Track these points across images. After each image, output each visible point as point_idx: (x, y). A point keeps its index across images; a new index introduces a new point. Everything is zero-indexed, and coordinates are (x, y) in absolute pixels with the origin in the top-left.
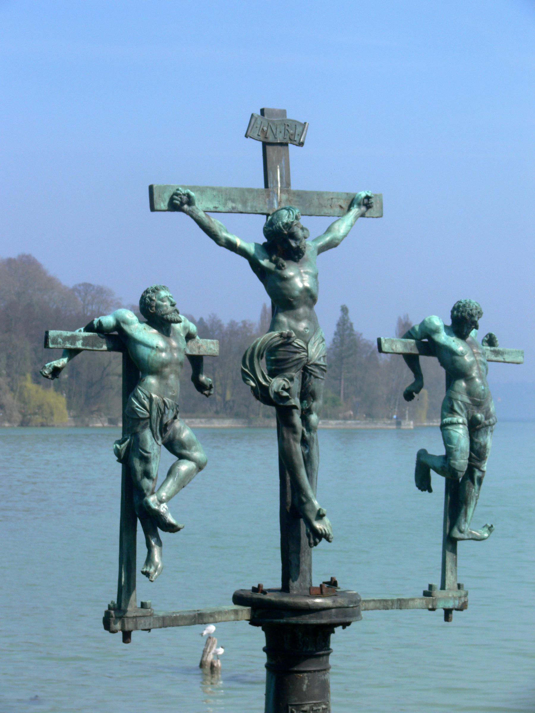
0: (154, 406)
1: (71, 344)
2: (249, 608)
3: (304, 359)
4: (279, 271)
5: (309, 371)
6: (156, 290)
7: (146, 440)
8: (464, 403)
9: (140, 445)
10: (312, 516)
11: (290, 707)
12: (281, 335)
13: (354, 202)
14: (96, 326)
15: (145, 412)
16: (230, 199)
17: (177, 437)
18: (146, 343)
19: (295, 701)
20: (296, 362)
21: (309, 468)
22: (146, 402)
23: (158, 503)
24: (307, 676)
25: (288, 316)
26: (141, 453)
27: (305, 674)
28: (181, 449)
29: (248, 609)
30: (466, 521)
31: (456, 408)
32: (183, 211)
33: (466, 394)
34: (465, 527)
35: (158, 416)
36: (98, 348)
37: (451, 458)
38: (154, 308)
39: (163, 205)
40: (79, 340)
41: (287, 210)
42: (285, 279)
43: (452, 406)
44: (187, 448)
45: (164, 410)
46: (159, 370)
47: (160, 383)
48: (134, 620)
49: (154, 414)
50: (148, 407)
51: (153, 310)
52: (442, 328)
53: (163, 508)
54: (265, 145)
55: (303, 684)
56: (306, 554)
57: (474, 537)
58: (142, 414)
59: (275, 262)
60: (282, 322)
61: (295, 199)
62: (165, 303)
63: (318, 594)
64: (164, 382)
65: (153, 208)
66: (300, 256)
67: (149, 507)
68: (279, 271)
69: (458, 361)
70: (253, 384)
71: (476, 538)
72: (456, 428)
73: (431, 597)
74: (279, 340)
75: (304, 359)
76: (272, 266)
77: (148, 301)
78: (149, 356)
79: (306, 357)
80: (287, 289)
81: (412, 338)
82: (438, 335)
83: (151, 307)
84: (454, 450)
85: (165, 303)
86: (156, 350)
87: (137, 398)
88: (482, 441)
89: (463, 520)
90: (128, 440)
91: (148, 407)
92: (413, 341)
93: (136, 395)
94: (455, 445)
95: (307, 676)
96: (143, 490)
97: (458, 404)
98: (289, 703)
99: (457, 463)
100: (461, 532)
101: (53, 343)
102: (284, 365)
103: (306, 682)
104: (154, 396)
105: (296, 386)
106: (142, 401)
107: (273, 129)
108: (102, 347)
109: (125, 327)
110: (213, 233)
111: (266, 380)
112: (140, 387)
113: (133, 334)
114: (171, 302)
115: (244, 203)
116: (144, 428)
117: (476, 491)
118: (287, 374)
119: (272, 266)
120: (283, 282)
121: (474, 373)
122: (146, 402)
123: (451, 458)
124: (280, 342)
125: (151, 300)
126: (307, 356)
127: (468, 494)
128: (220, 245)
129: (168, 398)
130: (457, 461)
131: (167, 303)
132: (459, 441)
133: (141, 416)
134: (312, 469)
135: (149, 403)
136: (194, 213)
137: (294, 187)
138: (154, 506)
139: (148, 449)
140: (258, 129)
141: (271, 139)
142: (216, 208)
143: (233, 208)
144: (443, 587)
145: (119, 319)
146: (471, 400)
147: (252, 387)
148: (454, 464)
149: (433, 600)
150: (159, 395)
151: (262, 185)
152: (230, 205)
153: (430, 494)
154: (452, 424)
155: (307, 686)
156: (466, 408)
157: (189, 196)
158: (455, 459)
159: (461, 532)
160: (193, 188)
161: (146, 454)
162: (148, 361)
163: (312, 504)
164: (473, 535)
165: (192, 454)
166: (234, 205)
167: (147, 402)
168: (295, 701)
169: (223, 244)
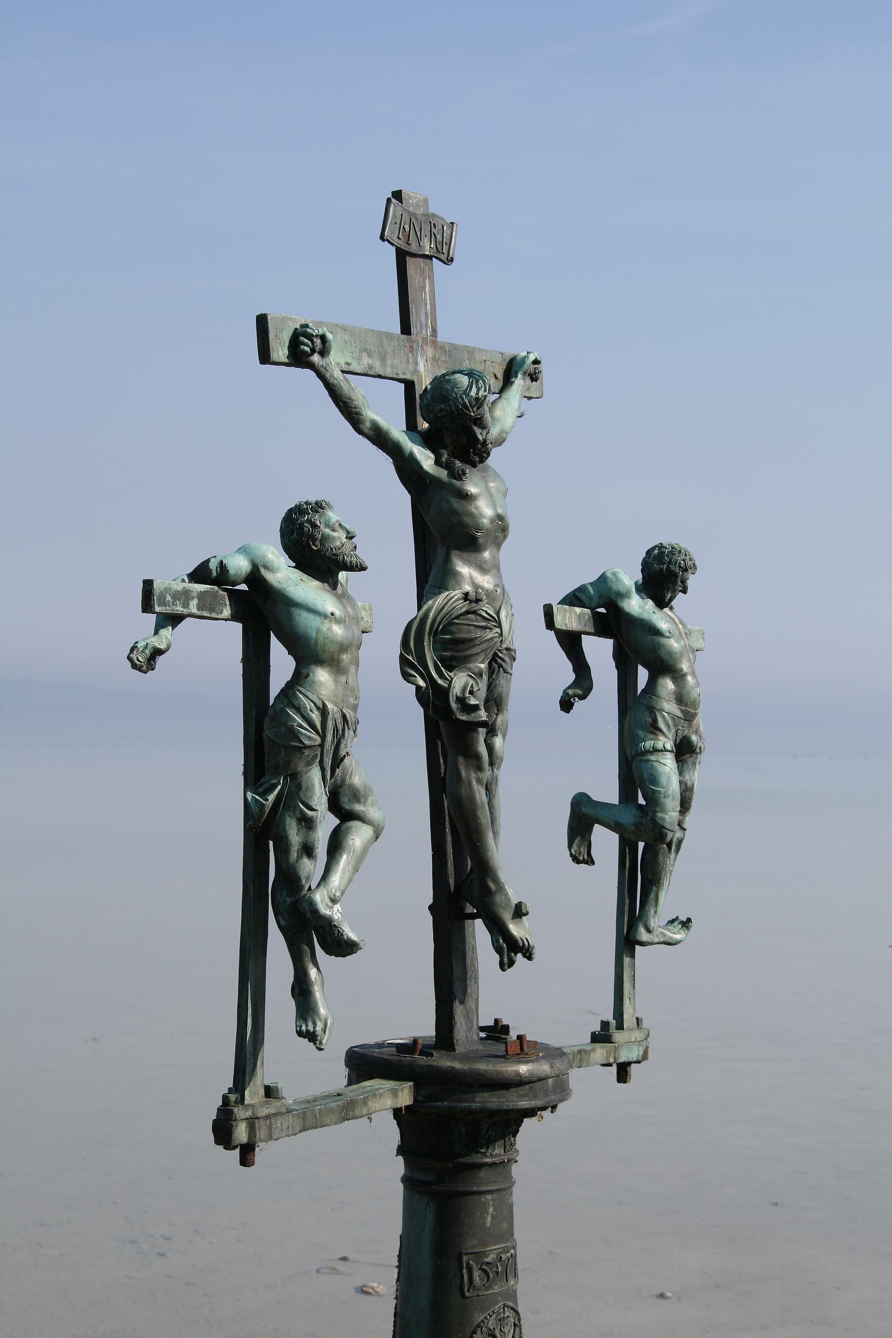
0: (330, 725)
1: (183, 607)
2: (411, 1084)
3: (495, 640)
4: (457, 483)
5: (499, 661)
6: (319, 507)
7: (313, 786)
8: (674, 717)
9: (302, 796)
10: (507, 916)
11: (465, 1258)
12: (466, 597)
13: (514, 368)
14: (214, 574)
15: (316, 736)
16: (365, 350)
17: (348, 781)
18: (312, 607)
19: (475, 1246)
20: (485, 646)
21: (369, 823)
22: (316, 717)
23: (330, 904)
24: (492, 1200)
25: (468, 562)
26: (301, 811)
27: (489, 1197)
28: (352, 802)
29: (410, 1086)
30: (656, 912)
31: (661, 725)
32: (311, 366)
33: (674, 701)
34: (655, 923)
35: (333, 742)
36: (218, 614)
37: (657, 809)
38: (318, 543)
39: (280, 352)
40: (193, 598)
41: (466, 375)
42: (467, 497)
43: (655, 721)
44: (362, 800)
45: (343, 730)
46: (336, 657)
47: (336, 682)
48: (268, 1122)
49: (329, 738)
50: (319, 727)
51: (317, 547)
52: (634, 589)
53: (335, 913)
54: (402, 256)
55: (486, 1215)
56: (473, 981)
57: (666, 939)
58: (310, 738)
59: (448, 466)
60: (460, 574)
61: (443, 358)
62: (335, 534)
63: (517, 1054)
64: (343, 679)
65: (265, 357)
66: (484, 457)
67: (315, 912)
68: (457, 483)
69: (663, 646)
70: (422, 683)
71: (670, 941)
72: (663, 758)
73: (613, 1044)
74: (464, 606)
75: (495, 640)
76: (443, 474)
77: (309, 529)
78: (318, 631)
79: (499, 637)
80: (471, 514)
81: (582, 605)
82: (629, 601)
83: (314, 539)
84: (662, 795)
85: (335, 534)
86: (331, 620)
87: (298, 710)
88: (687, 780)
89: (652, 912)
90: (279, 787)
91: (319, 727)
92: (587, 611)
93: (296, 703)
94: (663, 788)
95: (492, 1200)
96: (299, 879)
97: (664, 717)
98: (464, 1251)
99: (667, 817)
100: (649, 931)
101: (159, 605)
102: (467, 649)
103: (491, 1209)
104: (330, 706)
105: (482, 687)
106: (308, 714)
107: (417, 230)
108: (221, 612)
109: (269, 576)
110: (355, 410)
111: (442, 676)
112: (300, 688)
113: (285, 589)
114: (348, 532)
115: (383, 358)
116: (309, 764)
117: (672, 862)
118: (472, 665)
119: (443, 474)
120: (464, 502)
121: (685, 666)
122: (316, 717)
123: (657, 809)
124: (464, 609)
125: (314, 526)
126: (501, 635)
127: (662, 868)
128: (359, 431)
129: (349, 708)
130: (667, 814)
131: (341, 535)
132: (669, 780)
133: (307, 742)
134: (371, 822)
135: (320, 718)
136: (327, 370)
137: (441, 338)
138: (324, 910)
139: (313, 804)
140: (398, 226)
141: (414, 248)
142: (348, 364)
143: (371, 367)
144: (620, 1026)
145: (258, 561)
146: (682, 711)
147: (418, 688)
148: (663, 819)
149: (616, 1048)
150: (336, 704)
151: (396, 328)
152: (366, 361)
153: (592, 867)
154: (655, 750)
155: (493, 1218)
156: (675, 725)
157: (323, 338)
158: (664, 811)
159: (649, 931)
160: (334, 327)
161: (310, 813)
162: (316, 640)
163: (507, 895)
164: (665, 936)
165: (368, 811)
166: (370, 361)
167: (317, 717)
168: (475, 1246)
169: (366, 431)
